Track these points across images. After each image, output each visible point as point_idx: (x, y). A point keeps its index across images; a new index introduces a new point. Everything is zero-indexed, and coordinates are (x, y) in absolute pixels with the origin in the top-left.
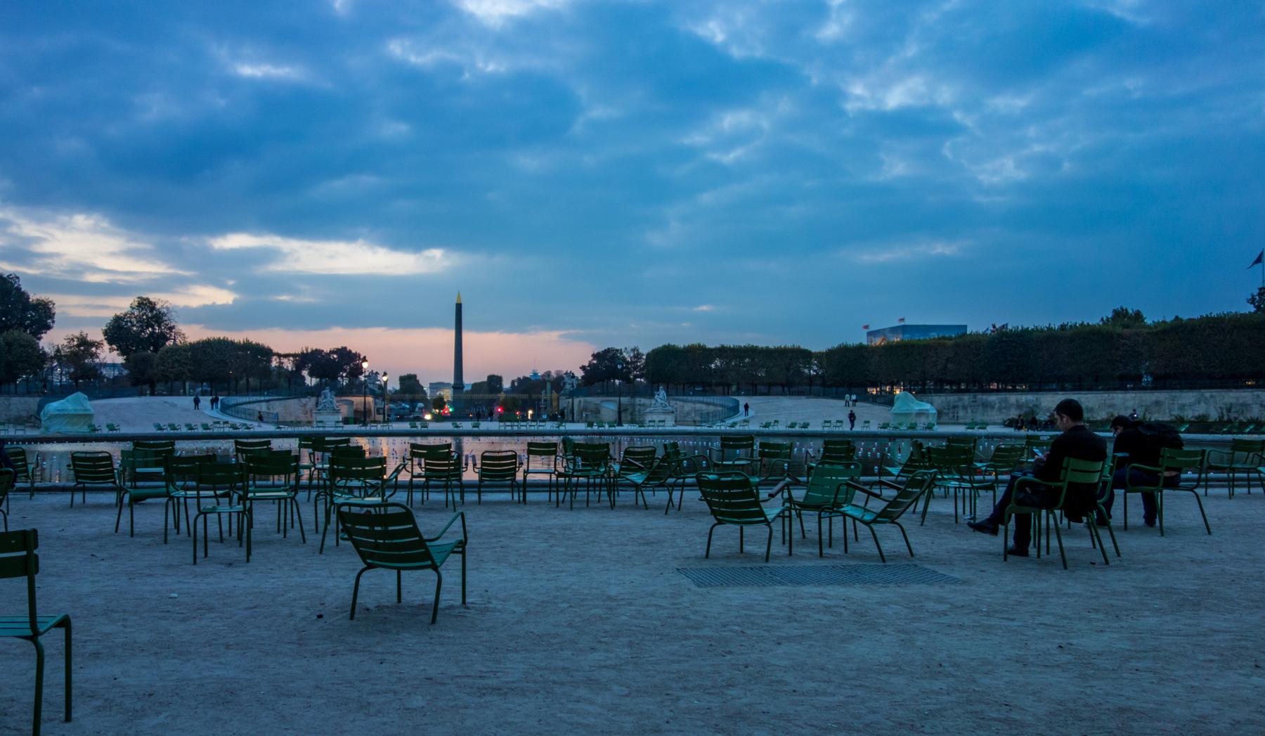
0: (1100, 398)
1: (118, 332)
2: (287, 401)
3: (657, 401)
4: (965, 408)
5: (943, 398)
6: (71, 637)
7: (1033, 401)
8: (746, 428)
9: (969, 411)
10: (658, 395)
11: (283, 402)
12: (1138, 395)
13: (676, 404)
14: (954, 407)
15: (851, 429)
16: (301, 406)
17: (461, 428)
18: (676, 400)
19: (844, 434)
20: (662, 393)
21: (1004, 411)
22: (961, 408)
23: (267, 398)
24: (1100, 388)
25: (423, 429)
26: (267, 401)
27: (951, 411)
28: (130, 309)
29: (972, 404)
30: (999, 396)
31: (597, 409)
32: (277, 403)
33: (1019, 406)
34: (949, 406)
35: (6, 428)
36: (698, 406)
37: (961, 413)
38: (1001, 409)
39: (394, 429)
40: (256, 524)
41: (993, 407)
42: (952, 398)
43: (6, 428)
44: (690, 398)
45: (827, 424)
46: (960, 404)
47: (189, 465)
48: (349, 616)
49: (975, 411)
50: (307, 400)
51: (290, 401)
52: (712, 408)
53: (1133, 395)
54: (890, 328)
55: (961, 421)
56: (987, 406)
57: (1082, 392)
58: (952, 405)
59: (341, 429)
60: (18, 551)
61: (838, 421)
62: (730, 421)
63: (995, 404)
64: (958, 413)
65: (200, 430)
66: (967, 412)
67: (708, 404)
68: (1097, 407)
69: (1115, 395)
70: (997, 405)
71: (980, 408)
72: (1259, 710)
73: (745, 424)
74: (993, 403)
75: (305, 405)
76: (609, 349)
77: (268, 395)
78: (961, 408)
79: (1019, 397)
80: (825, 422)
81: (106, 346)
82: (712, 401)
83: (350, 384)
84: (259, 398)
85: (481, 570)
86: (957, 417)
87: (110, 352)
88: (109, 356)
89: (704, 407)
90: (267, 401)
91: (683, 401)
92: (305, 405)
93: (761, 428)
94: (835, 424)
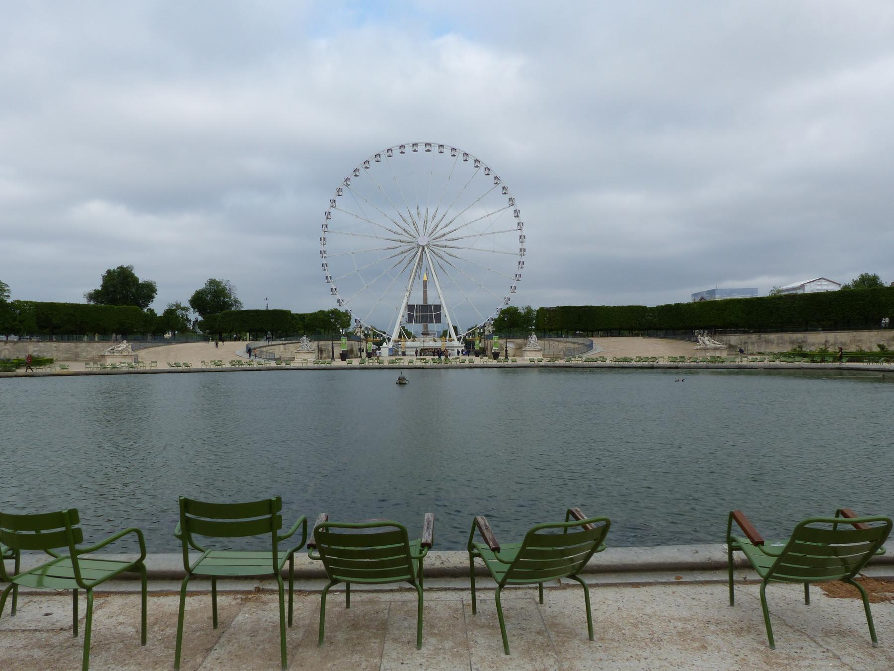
0: (851, 335)
1: (198, 301)
3: (530, 342)
4: (753, 343)
5: (737, 337)
6: (729, 518)
7: (801, 338)
9: (756, 345)
10: (531, 338)
11: (295, 344)
12: (880, 333)
13: (554, 343)
14: (745, 343)
15: (26, 371)
17: (190, 368)
18: (553, 341)
21: (780, 345)
22: (750, 344)
23: (284, 342)
24: (168, 335)
25: (410, 364)
26: (284, 344)
29: (758, 341)
30: (777, 335)
33: (792, 342)
35: (270, 363)
36: (568, 345)
37: (750, 347)
41: (772, 343)
42: (743, 336)
43: (270, 363)
44: (562, 339)
45: (153, 364)
46: (749, 341)
48: (565, 518)
52: (577, 346)
53: (876, 333)
54: (707, 291)
57: (838, 331)
58: (743, 342)
62: (585, 356)
63: (774, 341)
64: (748, 347)
65: (184, 368)
66: (754, 346)
67: (574, 343)
68: (849, 342)
71: (764, 343)
74: (772, 340)
77: (284, 340)
78: (750, 344)
80: (152, 362)
81: (192, 310)
82: (577, 341)
84: (278, 342)
85: (96, 493)
88: (194, 316)
89: (572, 345)
90: (284, 344)
91: (558, 341)
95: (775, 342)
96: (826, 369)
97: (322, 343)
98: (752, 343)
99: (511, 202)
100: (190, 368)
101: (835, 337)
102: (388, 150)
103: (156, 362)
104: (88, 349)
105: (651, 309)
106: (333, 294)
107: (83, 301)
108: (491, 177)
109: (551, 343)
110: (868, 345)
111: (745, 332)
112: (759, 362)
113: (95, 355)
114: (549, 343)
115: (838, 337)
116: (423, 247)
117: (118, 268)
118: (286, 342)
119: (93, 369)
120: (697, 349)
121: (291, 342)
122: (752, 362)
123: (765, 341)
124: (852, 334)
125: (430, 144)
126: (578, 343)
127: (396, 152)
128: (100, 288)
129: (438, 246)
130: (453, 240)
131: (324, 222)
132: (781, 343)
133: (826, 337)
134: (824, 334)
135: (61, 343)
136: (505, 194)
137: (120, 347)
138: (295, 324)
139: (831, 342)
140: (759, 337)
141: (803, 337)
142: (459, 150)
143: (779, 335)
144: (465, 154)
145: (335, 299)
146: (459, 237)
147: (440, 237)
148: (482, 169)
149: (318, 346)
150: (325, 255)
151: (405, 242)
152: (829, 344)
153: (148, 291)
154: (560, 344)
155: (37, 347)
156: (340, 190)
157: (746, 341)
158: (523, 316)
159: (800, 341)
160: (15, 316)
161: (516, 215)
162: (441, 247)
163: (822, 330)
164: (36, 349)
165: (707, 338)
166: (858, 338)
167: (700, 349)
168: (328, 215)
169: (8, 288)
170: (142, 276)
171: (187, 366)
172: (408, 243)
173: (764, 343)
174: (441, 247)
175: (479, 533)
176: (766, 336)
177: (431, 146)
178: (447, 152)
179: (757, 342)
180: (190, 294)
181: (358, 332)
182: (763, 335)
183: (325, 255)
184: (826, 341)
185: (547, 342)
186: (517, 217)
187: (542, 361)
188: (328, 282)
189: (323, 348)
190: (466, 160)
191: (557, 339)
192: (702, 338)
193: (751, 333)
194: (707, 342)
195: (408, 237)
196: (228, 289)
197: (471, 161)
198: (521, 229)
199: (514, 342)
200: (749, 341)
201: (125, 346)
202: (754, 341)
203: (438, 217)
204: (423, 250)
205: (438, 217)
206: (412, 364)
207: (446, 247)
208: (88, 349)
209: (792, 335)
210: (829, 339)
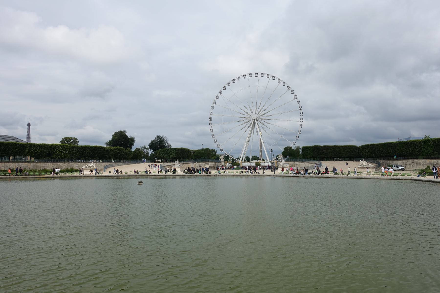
1: (153, 145)
4: (410, 165)
5: (401, 161)
9: (411, 166)
11: (188, 164)
14: (406, 164)
17: (102, 174)
20: (178, 161)
22: (408, 165)
23: (183, 163)
25: (229, 174)
26: (183, 164)
28: (155, 139)
29: (412, 163)
30: (422, 160)
34: (404, 164)
37: (408, 167)
38: (424, 165)
41: (420, 164)
42: (405, 161)
44: (311, 162)
46: (408, 163)
49: (413, 166)
50: (196, 163)
55: (408, 169)
56: (265, 161)
58: (405, 164)
59: (71, 175)
64: (407, 166)
70: (422, 163)
72: (401, 222)
74: (420, 163)
75: (195, 165)
76: (288, 147)
77: (183, 162)
78: (408, 165)
83: (89, 157)
86: (407, 168)
87: (327, 167)
88: (151, 152)
92: (195, 165)
93: (279, 174)
95: (422, 164)
96: (400, 179)
97: (200, 163)
99: (296, 97)
100: (102, 174)
102: (244, 75)
104: (99, 166)
106: (215, 142)
108: (286, 86)
109: (306, 164)
111: (405, 159)
113: (102, 168)
114: (305, 164)
116: (254, 120)
117: (119, 131)
118: (184, 163)
120: (359, 168)
121: (185, 163)
122: (402, 176)
123: (416, 163)
125: (251, 74)
126: (314, 163)
127: (242, 78)
128: (358, 146)
129: (261, 119)
130: (268, 116)
131: (211, 111)
132: (425, 165)
136: (293, 94)
137: (90, 165)
138: (190, 155)
141: (437, 162)
142: (271, 75)
143: (424, 160)
144: (273, 77)
145: (216, 145)
146: (271, 115)
147: (262, 115)
148: (282, 83)
149: (199, 165)
150: (211, 125)
151: (247, 118)
153: (131, 141)
154: (309, 164)
155: (78, 165)
156: (218, 96)
158: (295, 151)
159: (435, 164)
161: (298, 103)
162: (263, 119)
164: (77, 166)
165: (364, 162)
167: (360, 168)
168: (212, 107)
169: (77, 141)
170: (129, 135)
171: (101, 174)
173: (415, 165)
174: (263, 119)
176: (417, 161)
177: (269, 76)
178: (265, 76)
180: (149, 142)
183: (211, 125)
185: (304, 163)
186: (299, 104)
187: (238, 173)
188: (213, 137)
189: (201, 165)
190: (274, 80)
191: (308, 162)
192: (362, 162)
193: (422, 159)
194: (365, 164)
195: (249, 116)
196: (165, 140)
197: (276, 80)
198: (300, 110)
199: (289, 163)
200: (408, 163)
201: (93, 164)
202: (410, 163)
203: (262, 105)
204: (254, 121)
205: (262, 105)
206: (237, 174)
207: (265, 119)
208: (99, 166)
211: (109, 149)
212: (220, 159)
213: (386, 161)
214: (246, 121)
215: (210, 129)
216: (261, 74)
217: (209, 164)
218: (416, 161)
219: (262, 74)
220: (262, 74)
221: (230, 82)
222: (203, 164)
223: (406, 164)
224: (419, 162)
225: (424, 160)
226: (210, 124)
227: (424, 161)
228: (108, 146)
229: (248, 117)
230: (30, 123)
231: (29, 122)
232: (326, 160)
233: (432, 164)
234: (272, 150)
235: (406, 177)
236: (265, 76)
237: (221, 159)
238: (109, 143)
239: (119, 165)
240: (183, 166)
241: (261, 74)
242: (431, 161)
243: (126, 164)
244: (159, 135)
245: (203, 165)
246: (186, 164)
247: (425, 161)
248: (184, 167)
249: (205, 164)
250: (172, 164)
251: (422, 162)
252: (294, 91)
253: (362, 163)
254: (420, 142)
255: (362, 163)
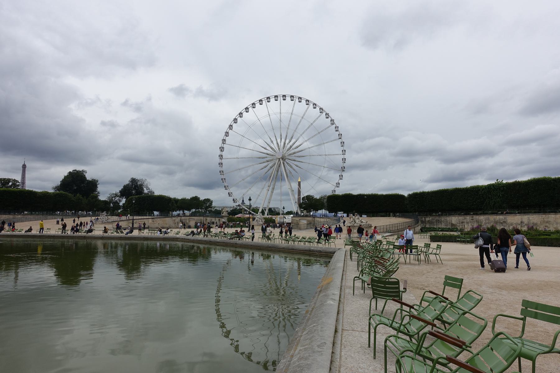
1: (126, 191)
2: (164, 218)
4: (468, 223)
5: (457, 218)
8: (49, 233)
14: (462, 223)
16: (172, 221)
19: (94, 237)
22: (465, 223)
27: (461, 224)
29: (471, 221)
30: (485, 217)
31: (297, 223)
32: (159, 219)
34: (460, 222)
39: (96, 234)
40: (372, 311)
46: (465, 221)
47: (9, 255)
50: (176, 218)
51: (166, 218)
57: (530, 214)
58: (461, 221)
60: (444, 338)
61: (48, 229)
66: (469, 225)
68: (539, 223)
69: (550, 216)
73: (48, 230)
74: (481, 221)
75: (174, 220)
79: (495, 217)
93: (174, 235)
94: (46, 231)
98: (467, 222)
101: (529, 219)
103: (50, 229)
105: (384, 195)
107: (51, 191)
110: (555, 226)
112: (83, 233)
115: (531, 218)
116: (279, 159)
119: (58, 233)
123: (476, 221)
124: (542, 217)
125: (293, 96)
133: (521, 219)
134: (520, 216)
135: (2, 215)
138: (171, 206)
139: (525, 223)
140: (472, 218)
141: (504, 219)
143: (486, 217)
149: (181, 220)
152: (524, 224)
157: (463, 221)
159: (502, 222)
160: (519, 208)
163: (518, 213)
166: (546, 220)
172: (272, 156)
173: (475, 223)
175: (457, 367)
176: (477, 217)
178: (288, 99)
179: (471, 222)
181: (224, 212)
182: (475, 217)
184: (521, 222)
192: (353, 217)
197: (304, 102)
205: (273, 139)
209: (496, 217)
210: (524, 220)
211: (58, 194)
212: (223, 213)
213: (437, 218)
214: (268, 159)
215: (220, 171)
216: (282, 96)
217: (194, 219)
218: (476, 218)
219: (292, 96)
220: (284, 96)
221: (248, 106)
222: (186, 220)
223: (462, 223)
224: (480, 220)
225: (486, 217)
226: (219, 164)
227: (487, 218)
228: (58, 192)
229: (272, 154)
230: (25, 164)
231: (24, 163)
232: (375, 216)
233: (498, 222)
234: (251, 198)
235: (307, 245)
236: (288, 99)
237: (224, 213)
238: (57, 188)
239: (51, 218)
240: (153, 222)
241: (291, 97)
242: (497, 218)
243: (70, 217)
244: (134, 178)
245: (186, 221)
246: (159, 219)
247: (488, 218)
248: (155, 223)
249: (189, 219)
250: (137, 218)
251: (484, 220)
252: (335, 121)
253: (354, 219)
254: (483, 190)
255: (354, 219)
